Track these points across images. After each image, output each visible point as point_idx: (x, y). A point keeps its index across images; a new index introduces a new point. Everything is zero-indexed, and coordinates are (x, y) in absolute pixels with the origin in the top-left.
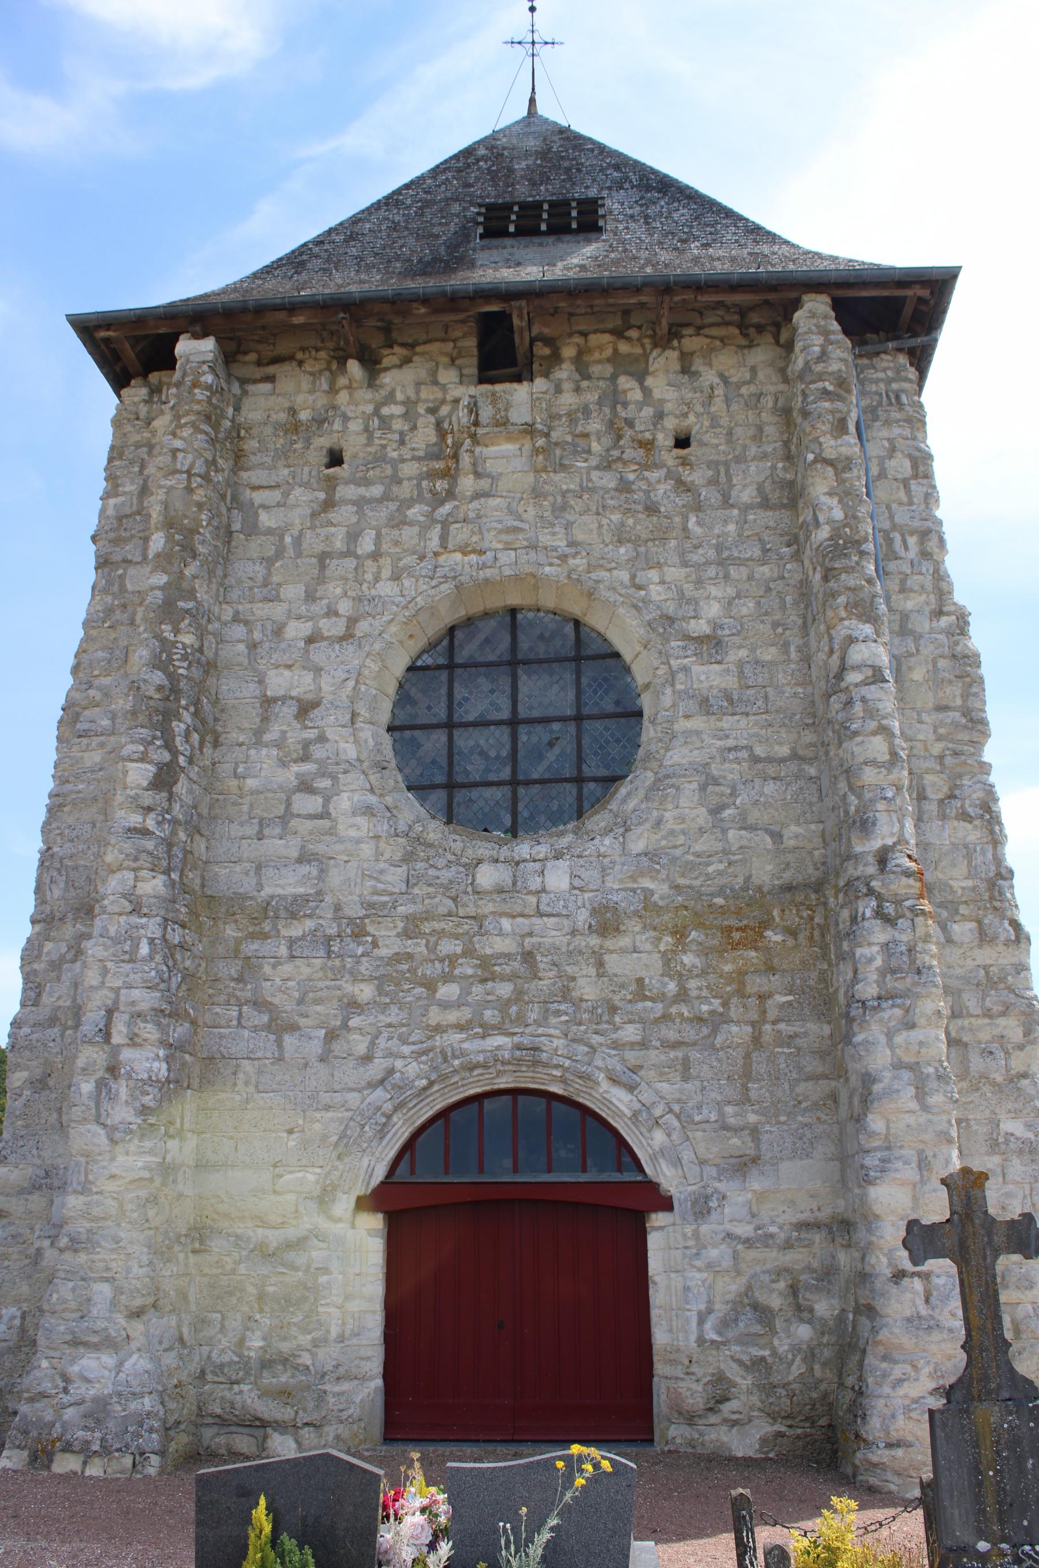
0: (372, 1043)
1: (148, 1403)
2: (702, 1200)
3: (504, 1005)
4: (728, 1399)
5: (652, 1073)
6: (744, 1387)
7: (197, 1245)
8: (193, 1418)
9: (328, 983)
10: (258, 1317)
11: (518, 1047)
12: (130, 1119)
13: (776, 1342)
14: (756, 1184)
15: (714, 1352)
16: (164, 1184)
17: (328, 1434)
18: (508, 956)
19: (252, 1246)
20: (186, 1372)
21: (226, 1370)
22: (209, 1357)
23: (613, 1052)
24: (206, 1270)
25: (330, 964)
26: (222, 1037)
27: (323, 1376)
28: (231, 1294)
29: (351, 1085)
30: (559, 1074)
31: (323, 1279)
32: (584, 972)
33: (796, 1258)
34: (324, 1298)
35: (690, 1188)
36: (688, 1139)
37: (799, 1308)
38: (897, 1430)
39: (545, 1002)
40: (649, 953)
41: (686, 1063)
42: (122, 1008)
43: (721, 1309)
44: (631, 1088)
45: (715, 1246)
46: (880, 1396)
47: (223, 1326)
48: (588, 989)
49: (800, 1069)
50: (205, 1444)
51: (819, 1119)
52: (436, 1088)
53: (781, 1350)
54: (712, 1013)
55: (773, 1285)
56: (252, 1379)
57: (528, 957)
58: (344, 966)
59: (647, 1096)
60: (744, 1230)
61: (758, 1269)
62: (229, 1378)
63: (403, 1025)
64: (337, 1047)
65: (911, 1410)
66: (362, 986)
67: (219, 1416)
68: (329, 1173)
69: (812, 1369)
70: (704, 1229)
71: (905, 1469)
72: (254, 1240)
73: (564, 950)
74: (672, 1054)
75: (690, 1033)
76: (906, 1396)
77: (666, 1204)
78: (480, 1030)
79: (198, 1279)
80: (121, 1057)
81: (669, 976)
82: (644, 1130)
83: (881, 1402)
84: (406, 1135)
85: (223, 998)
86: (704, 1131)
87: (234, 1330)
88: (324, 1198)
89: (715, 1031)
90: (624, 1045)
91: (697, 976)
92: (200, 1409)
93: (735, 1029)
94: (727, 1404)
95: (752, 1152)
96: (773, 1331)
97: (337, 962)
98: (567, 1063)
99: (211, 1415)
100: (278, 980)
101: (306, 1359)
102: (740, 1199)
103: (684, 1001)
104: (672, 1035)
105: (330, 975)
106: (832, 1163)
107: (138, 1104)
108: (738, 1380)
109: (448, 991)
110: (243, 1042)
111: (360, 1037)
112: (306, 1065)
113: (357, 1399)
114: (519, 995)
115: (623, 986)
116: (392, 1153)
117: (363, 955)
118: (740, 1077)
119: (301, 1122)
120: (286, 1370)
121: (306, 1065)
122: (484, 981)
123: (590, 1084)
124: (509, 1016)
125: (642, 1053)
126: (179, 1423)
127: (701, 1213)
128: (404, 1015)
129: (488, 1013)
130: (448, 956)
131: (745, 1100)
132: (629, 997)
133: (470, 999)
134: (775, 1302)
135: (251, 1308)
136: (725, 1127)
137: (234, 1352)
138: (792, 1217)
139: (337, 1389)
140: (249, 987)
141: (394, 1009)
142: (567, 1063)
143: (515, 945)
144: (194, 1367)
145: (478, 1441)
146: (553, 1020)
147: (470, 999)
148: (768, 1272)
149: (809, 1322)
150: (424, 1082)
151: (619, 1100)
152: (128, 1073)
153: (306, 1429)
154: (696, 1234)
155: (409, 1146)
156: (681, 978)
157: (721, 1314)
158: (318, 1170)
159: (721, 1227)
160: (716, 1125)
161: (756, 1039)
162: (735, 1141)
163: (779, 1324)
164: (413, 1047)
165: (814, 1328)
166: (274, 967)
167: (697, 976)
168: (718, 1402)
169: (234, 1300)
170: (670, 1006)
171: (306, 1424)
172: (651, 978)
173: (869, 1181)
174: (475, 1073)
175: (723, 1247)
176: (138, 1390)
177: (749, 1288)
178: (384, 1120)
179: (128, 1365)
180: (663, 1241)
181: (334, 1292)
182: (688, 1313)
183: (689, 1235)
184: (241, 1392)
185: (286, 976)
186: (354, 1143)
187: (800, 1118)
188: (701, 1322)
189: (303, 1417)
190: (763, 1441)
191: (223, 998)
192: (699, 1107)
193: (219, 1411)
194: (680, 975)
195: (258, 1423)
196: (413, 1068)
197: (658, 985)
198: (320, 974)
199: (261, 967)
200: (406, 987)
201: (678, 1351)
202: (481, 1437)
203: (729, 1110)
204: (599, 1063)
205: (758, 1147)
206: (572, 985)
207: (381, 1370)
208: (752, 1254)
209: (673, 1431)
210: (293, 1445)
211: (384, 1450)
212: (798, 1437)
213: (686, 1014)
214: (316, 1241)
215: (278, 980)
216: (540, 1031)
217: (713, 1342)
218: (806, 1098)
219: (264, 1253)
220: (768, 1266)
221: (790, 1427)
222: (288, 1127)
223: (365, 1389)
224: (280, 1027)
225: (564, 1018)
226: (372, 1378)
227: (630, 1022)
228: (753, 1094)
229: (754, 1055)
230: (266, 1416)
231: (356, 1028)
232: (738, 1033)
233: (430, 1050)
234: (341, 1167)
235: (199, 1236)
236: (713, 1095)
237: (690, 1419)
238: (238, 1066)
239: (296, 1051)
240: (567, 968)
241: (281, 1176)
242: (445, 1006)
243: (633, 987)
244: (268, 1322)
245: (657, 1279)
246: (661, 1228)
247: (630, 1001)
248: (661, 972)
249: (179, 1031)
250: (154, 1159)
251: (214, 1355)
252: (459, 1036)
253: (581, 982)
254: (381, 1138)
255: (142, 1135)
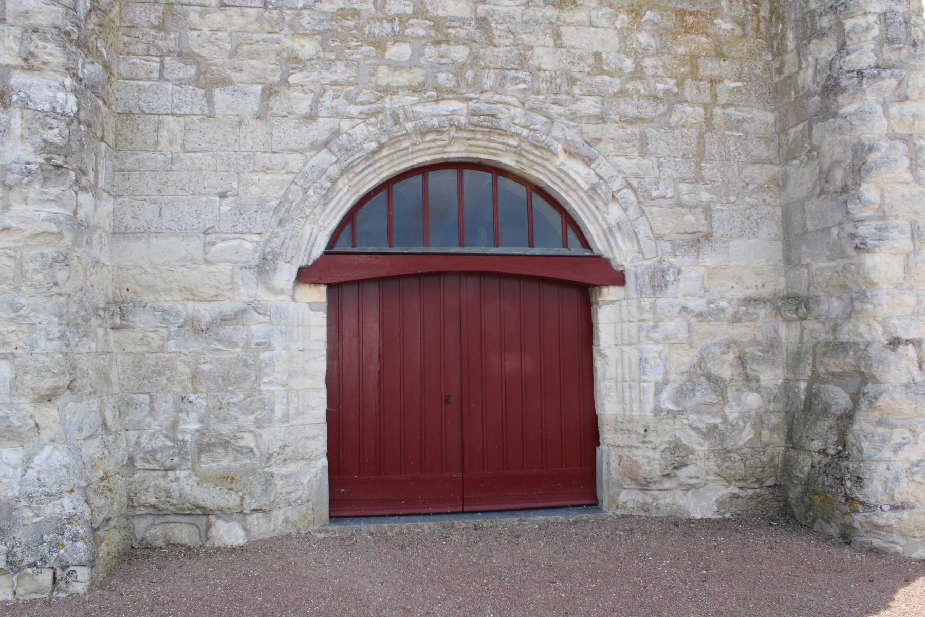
0: (316, 102)
1: (68, 504)
2: (660, 274)
3: (459, 69)
4: (685, 465)
5: (611, 146)
6: (701, 453)
7: (118, 321)
8: (124, 511)
9: (265, 36)
10: (192, 397)
11: (474, 113)
12: (28, 159)
13: (727, 410)
14: (709, 259)
15: (671, 421)
16: (76, 243)
17: (277, 519)
18: (463, 21)
19: (182, 321)
20: (112, 462)
21: (158, 456)
22: (137, 443)
23: (572, 124)
24: (130, 348)
25: (266, 14)
26: (140, 90)
27: (269, 459)
28: (159, 373)
29: (293, 145)
30: (515, 144)
31: (265, 355)
32: (542, 42)
33: (742, 332)
34: (267, 375)
35: (649, 262)
36: (643, 212)
37: (747, 378)
38: (901, 493)
39: (502, 69)
40: (606, 29)
41: (644, 141)
42: (10, 20)
43: (676, 380)
44: (588, 161)
45: (672, 319)
46: (879, 461)
47: (152, 409)
48: (546, 58)
49: (748, 153)
50: (139, 537)
51: (764, 201)
52: (385, 152)
53: (731, 418)
54: (667, 92)
55: (724, 357)
56: (189, 464)
57: (483, 23)
58: (283, 19)
59: (605, 170)
60: (697, 304)
61: (709, 342)
62: (163, 465)
63: (350, 84)
64: (276, 104)
65: (913, 474)
66: (303, 41)
67: (154, 506)
68: (269, 240)
69: (760, 434)
70: (662, 302)
71: (910, 531)
72: (184, 314)
73: (518, 19)
74: (629, 130)
75: (648, 110)
76: (907, 459)
77: (619, 279)
78: (434, 93)
79: (120, 358)
80: (12, 82)
81: (624, 52)
82: (600, 204)
83: (882, 466)
84: (350, 204)
85: (141, 47)
86: (660, 206)
87: (165, 412)
88: (263, 267)
89: (670, 110)
90: (581, 117)
91: (653, 55)
92: (130, 499)
93: (688, 109)
94: (684, 469)
95: (704, 229)
96: (724, 400)
97: (275, 14)
98: (525, 132)
99: (144, 506)
100: (206, 30)
101: (248, 441)
102: (693, 273)
103: (640, 78)
104: (631, 111)
105: (267, 27)
106: (775, 243)
107: (37, 139)
108: (695, 447)
109: (399, 51)
110: (165, 96)
111: (302, 95)
112: (241, 123)
113: (305, 480)
114: (475, 59)
115: (581, 58)
116: (334, 223)
117: (304, 8)
118: (694, 156)
119: (235, 184)
120: (227, 454)
121: (241, 123)
122: (438, 43)
123: (547, 155)
124: (466, 80)
125: (600, 126)
126: (110, 519)
127: (659, 286)
128: (351, 72)
129: (442, 77)
130: (398, 15)
131: (698, 179)
132: (588, 70)
133: (422, 60)
134: (726, 372)
135: (184, 388)
136: (680, 204)
137: (167, 437)
138: (740, 292)
139: (284, 471)
140: (172, 36)
141: (340, 66)
142: (525, 132)
143: (468, 10)
144: (121, 454)
145: (428, 514)
146: (510, 88)
147: (422, 60)
148: (719, 344)
149: (757, 390)
150: (374, 145)
151: (577, 173)
152: (22, 100)
153: (255, 515)
154: (653, 307)
155: (350, 218)
156: (638, 55)
157: (676, 385)
158: (256, 238)
159: (677, 301)
160: (672, 202)
161: (708, 120)
162: (689, 218)
163: (730, 393)
164: (362, 108)
165: (762, 397)
166: (202, 15)
167: (653, 55)
168: (676, 468)
169: (164, 380)
170: (627, 81)
171: (255, 510)
172: (608, 53)
173: (862, 248)
174: (429, 137)
175: (678, 320)
176: (54, 489)
177: (702, 359)
178: (329, 184)
179: (38, 460)
180: (611, 314)
181: (278, 369)
182: (645, 384)
183: (647, 308)
184: (177, 479)
185: (215, 27)
186: (297, 208)
187: (747, 199)
188: (658, 392)
189: (250, 503)
190: (720, 503)
191: (141, 47)
192: (657, 183)
193: (153, 501)
194: (637, 53)
195: (199, 511)
196: (361, 131)
197: (615, 60)
198: (255, 26)
199: (186, 15)
200: (353, 44)
201: (631, 420)
202: (431, 510)
203: (684, 187)
204: (557, 133)
205: (710, 225)
206: (529, 53)
207: (325, 448)
208: (703, 327)
209: (623, 497)
210: (241, 533)
211: (336, 529)
212: (751, 498)
213: (642, 91)
214: (256, 314)
215: (206, 30)
216: (497, 98)
217: (669, 411)
218: (753, 180)
219: (197, 328)
220: (718, 339)
221: (741, 488)
222: (220, 190)
223: (312, 471)
224: (209, 81)
225: (522, 86)
226: (318, 458)
227: (590, 94)
228: (706, 173)
229: (707, 135)
230: (208, 504)
231: (297, 85)
232: (692, 113)
233: (380, 112)
234: (282, 234)
235: (119, 311)
236: (670, 172)
237: (644, 484)
238: (161, 122)
239: (228, 107)
240: (524, 37)
241: (214, 244)
242: (395, 67)
243: (591, 60)
244: (204, 402)
245: (607, 352)
246: (612, 302)
247: (589, 74)
248: (617, 48)
249: (91, 70)
250: (62, 211)
251: (143, 440)
252: (410, 99)
253: (539, 51)
254: (325, 205)
255: (45, 179)
